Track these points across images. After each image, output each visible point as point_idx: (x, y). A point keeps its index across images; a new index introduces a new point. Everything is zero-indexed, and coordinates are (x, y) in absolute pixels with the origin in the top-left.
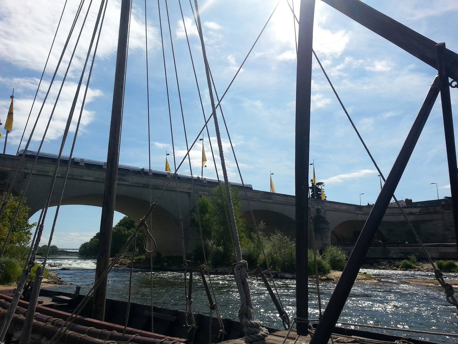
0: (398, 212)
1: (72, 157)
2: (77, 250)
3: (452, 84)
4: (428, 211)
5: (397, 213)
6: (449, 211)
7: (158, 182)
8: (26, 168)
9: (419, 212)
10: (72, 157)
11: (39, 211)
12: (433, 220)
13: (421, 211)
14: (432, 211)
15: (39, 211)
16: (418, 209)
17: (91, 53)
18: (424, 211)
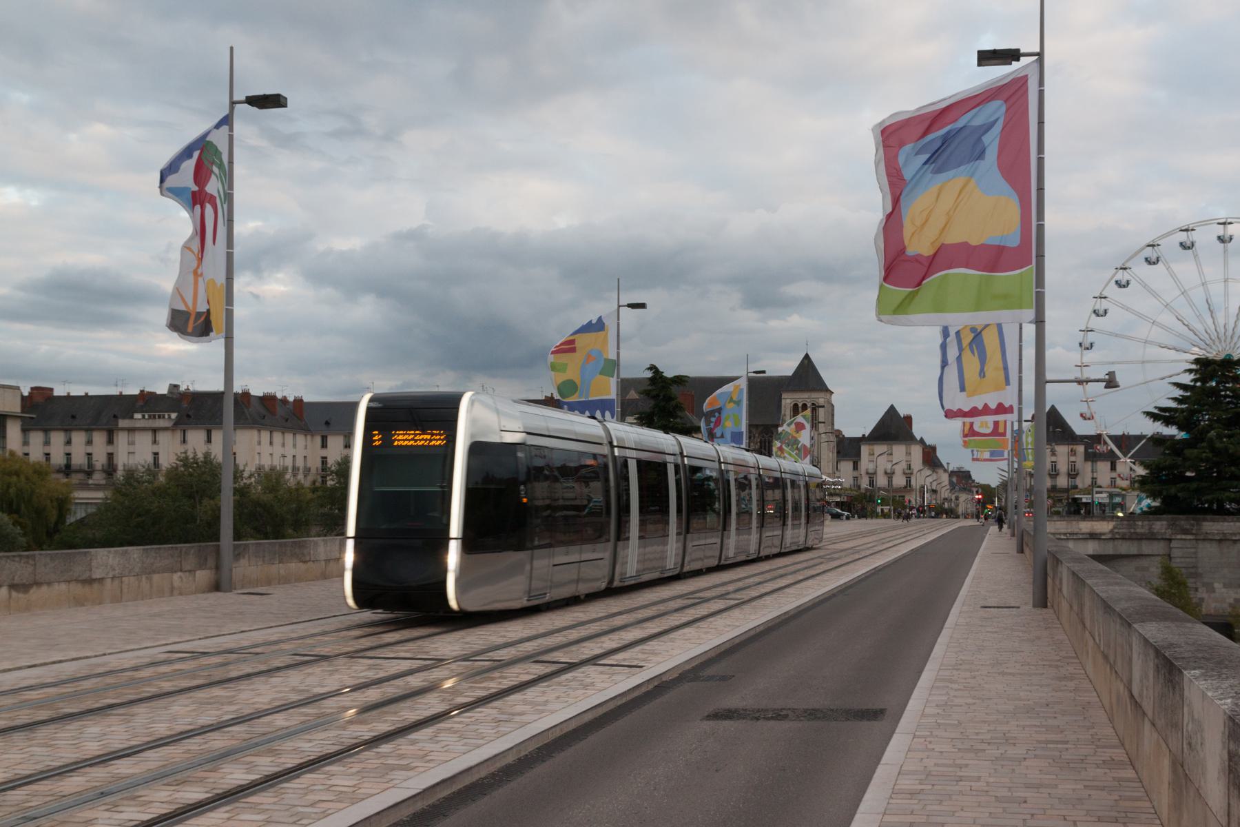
0: (1065, 531)
1: (208, 139)
2: (1183, 288)
3: (1019, 246)
4: (1132, 531)
5: (1065, 534)
6: (1189, 537)
7: (569, 491)
8: (972, 822)
9: (1111, 531)
10: (208, 139)
11: (87, 394)
12: (1142, 555)
13: (1116, 531)
14: (1143, 531)
15: (87, 394)
16: (1110, 523)
17: (605, 628)
18: (1124, 531)
